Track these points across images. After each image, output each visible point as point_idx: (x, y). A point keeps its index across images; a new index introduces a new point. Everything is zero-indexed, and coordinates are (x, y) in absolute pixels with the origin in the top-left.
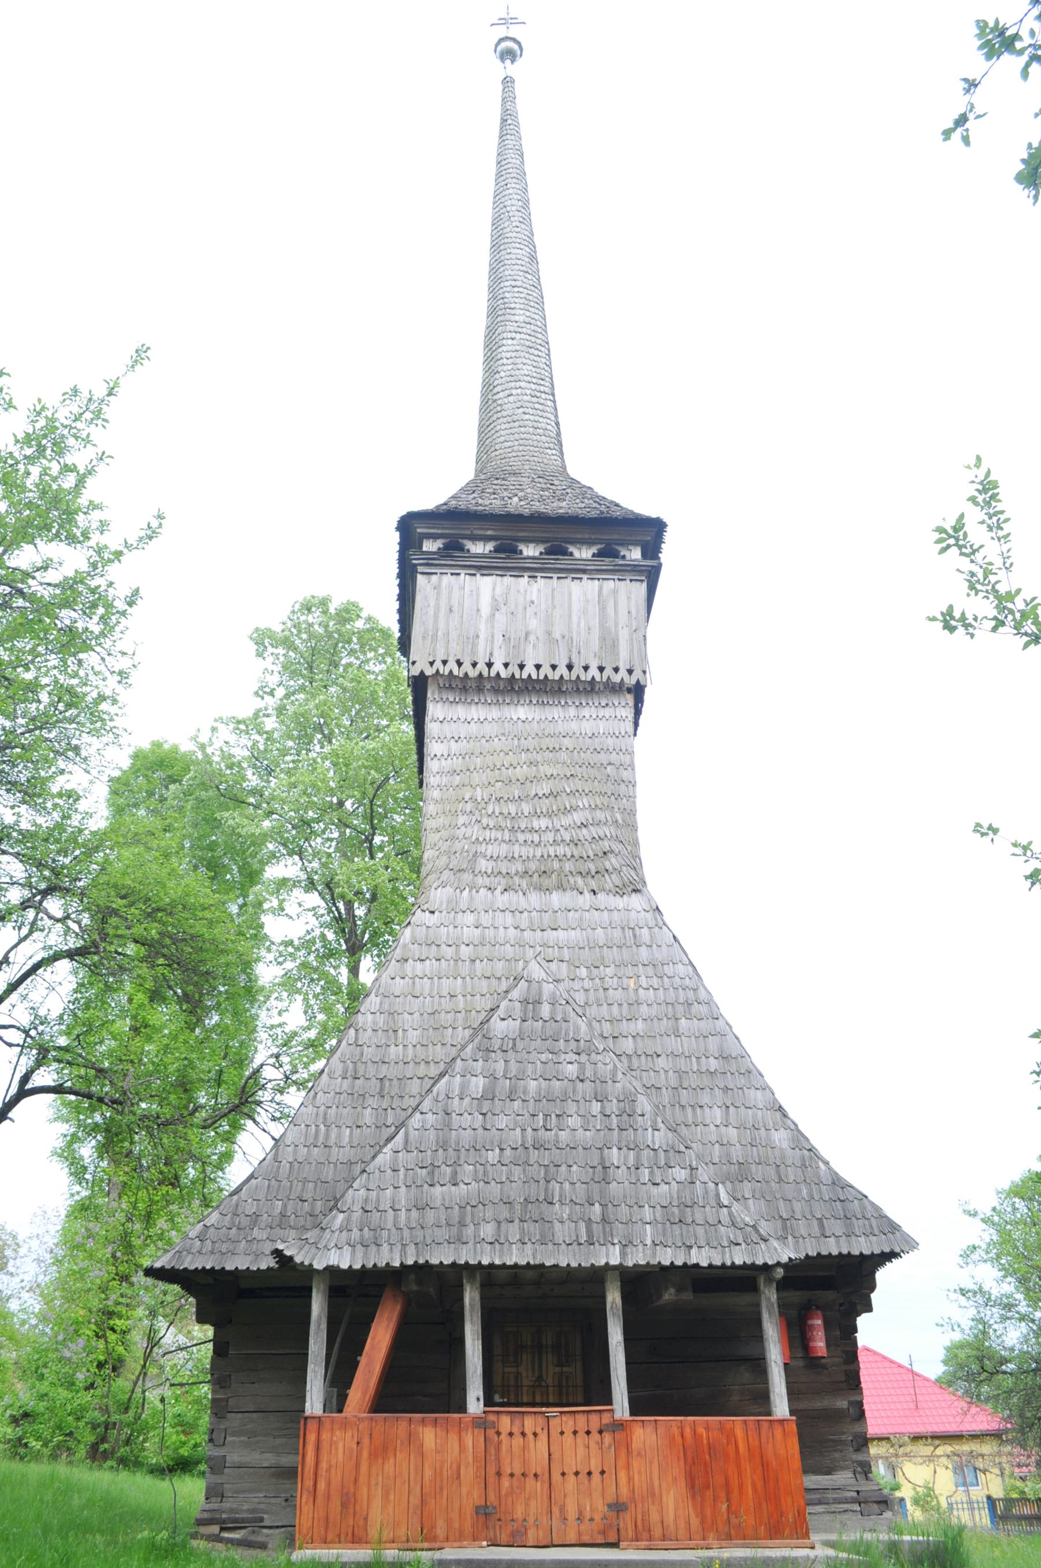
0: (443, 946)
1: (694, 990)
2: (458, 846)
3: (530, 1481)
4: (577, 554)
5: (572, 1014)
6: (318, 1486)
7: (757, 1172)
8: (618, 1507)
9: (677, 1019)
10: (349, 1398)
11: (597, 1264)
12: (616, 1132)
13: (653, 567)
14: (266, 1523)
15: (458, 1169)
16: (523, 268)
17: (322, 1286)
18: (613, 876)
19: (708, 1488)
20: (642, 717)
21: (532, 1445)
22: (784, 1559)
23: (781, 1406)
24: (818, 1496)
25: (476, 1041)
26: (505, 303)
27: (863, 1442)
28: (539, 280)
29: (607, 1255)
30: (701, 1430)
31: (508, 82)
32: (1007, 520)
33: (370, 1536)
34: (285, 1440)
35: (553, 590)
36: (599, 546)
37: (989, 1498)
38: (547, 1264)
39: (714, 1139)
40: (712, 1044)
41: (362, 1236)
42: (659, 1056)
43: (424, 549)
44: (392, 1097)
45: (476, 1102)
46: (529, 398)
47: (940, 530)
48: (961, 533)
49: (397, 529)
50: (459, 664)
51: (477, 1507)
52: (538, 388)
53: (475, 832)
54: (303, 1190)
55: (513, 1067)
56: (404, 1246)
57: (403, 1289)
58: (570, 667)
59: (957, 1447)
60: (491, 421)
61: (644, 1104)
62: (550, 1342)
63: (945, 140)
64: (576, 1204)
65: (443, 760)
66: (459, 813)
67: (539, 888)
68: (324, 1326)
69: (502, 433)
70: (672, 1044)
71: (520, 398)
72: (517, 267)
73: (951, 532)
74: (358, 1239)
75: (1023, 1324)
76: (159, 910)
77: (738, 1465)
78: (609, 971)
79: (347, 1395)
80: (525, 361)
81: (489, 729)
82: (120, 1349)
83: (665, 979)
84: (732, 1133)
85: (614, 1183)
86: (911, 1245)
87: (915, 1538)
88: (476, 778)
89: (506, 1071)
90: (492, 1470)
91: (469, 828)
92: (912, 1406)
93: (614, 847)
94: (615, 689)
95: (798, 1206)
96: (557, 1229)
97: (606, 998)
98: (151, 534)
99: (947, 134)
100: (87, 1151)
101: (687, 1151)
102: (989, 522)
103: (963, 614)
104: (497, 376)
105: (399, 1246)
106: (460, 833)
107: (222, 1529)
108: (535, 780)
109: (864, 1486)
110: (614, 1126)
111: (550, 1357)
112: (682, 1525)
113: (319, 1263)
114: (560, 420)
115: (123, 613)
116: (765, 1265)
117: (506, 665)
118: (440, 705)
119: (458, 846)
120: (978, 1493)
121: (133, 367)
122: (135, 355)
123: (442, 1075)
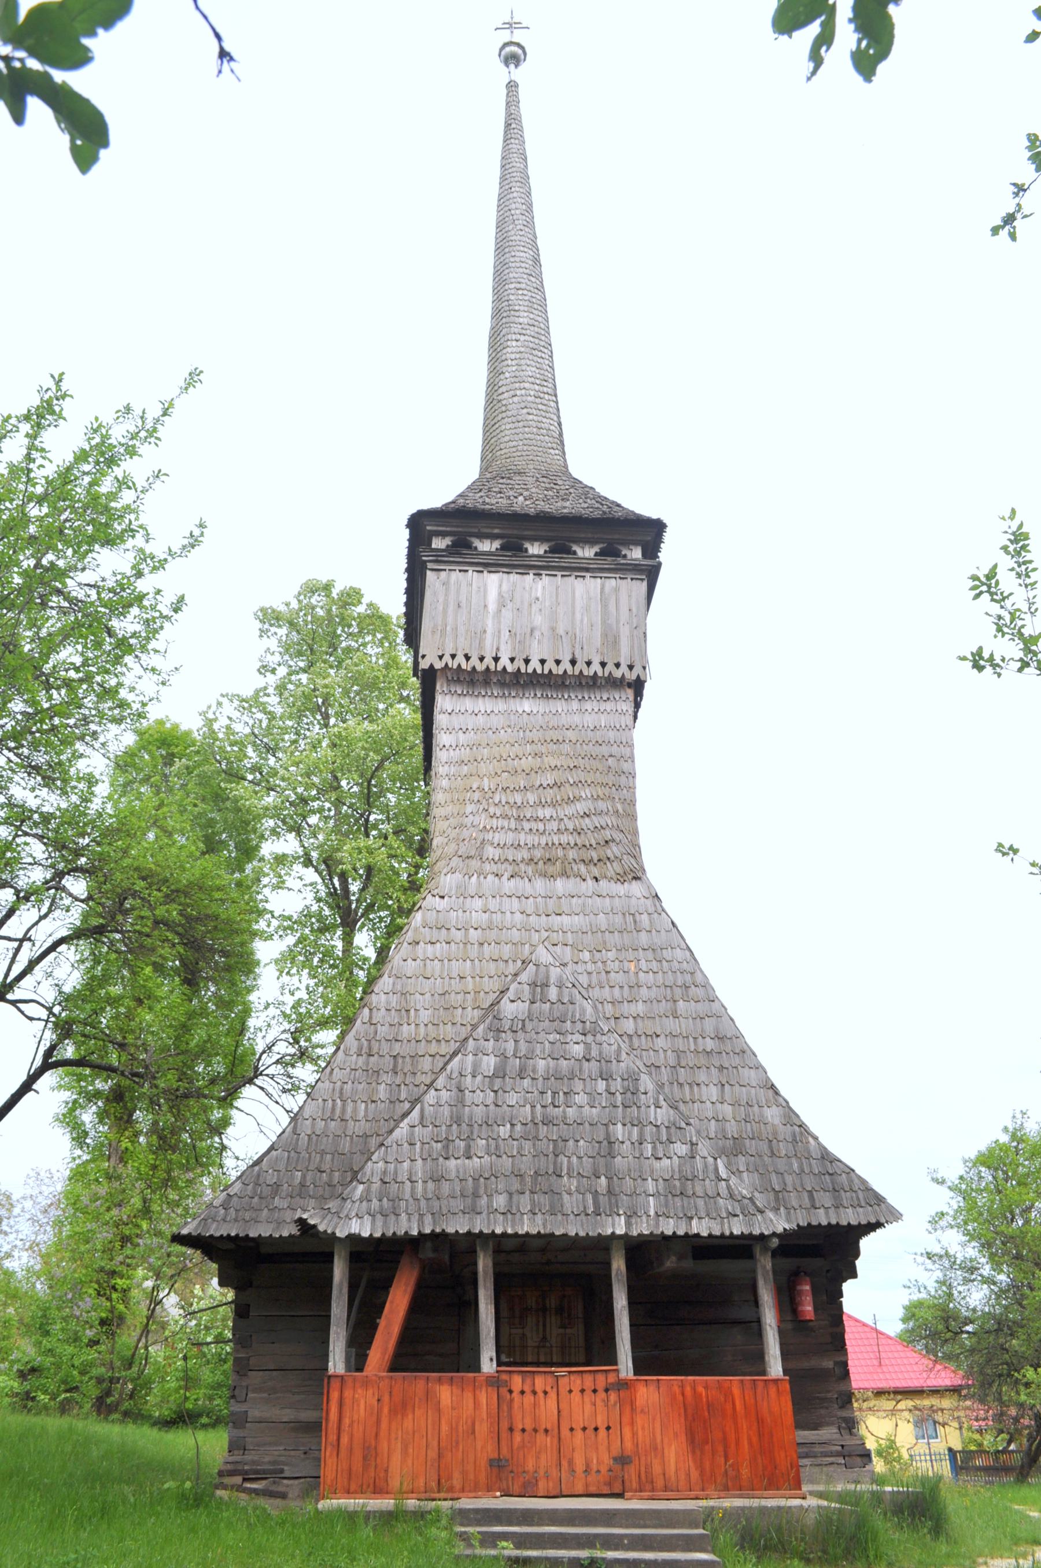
0: (453, 930)
1: (692, 974)
2: (466, 833)
3: (540, 1437)
4: (580, 553)
5: (578, 996)
6: (342, 1440)
7: (751, 1146)
8: (623, 1460)
9: (675, 1001)
10: (369, 1358)
11: (603, 1234)
12: (620, 1109)
13: (653, 566)
14: (287, 1474)
15: (472, 1143)
16: (527, 271)
17: (343, 1253)
18: (615, 864)
19: (707, 1443)
20: (640, 710)
21: (542, 1402)
22: (779, 1508)
23: (775, 1368)
24: (805, 1450)
25: (488, 1021)
26: (509, 305)
27: (847, 1399)
28: (542, 282)
29: (613, 1225)
30: (701, 1389)
31: (512, 87)
32: (1034, 570)
33: (390, 1487)
34: (303, 1396)
35: (557, 588)
36: (602, 546)
37: (950, 1450)
38: (557, 1233)
39: (710, 1115)
40: (709, 1025)
41: (381, 1206)
42: (658, 1036)
43: (434, 546)
44: (405, 1074)
45: (487, 1079)
46: (532, 399)
47: (975, 578)
48: (993, 581)
49: (408, 526)
50: (467, 658)
51: (491, 1460)
52: (541, 389)
53: (482, 820)
54: (321, 1161)
55: (523, 1047)
56: (421, 1216)
57: (421, 1256)
58: (573, 662)
59: (918, 1402)
60: (495, 420)
61: (647, 1082)
62: (553, 1306)
63: (993, 235)
64: (583, 1176)
65: (451, 751)
66: (468, 802)
67: (544, 875)
68: (345, 1290)
69: (507, 432)
70: (671, 1024)
71: (524, 398)
72: (521, 270)
73: (984, 579)
74: (377, 1209)
75: (985, 1286)
76: (177, 891)
77: (736, 1423)
78: (611, 955)
79: (367, 1355)
80: (529, 362)
81: (495, 721)
82: (121, 1307)
83: (664, 962)
84: (727, 1110)
85: (619, 1157)
86: (895, 1216)
87: (895, 1489)
88: (483, 768)
89: (516, 1050)
90: (505, 1425)
91: (477, 816)
92: (876, 1362)
93: (615, 836)
94: (615, 684)
95: (789, 1179)
96: (565, 1201)
97: (608, 980)
98: (194, 542)
99: (995, 231)
100: (88, 1117)
101: (688, 1128)
102: (1018, 570)
103: (992, 655)
104: (502, 377)
105: (417, 1216)
106: (468, 821)
107: (245, 1480)
108: (540, 771)
109: (849, 1441)
110: (619, 1103)
111: (553, 1318)
112: (683, 1477)
113: (341, 1231)
114: (562, 420)
115: (167, 618)
116: (762, 1235)
117: (512, 660)
118: (448, 697)
119: (466, 833)
120: (939, 1446)
121: (186, 389)
122: (188, 378)
123: (455, 1054)
